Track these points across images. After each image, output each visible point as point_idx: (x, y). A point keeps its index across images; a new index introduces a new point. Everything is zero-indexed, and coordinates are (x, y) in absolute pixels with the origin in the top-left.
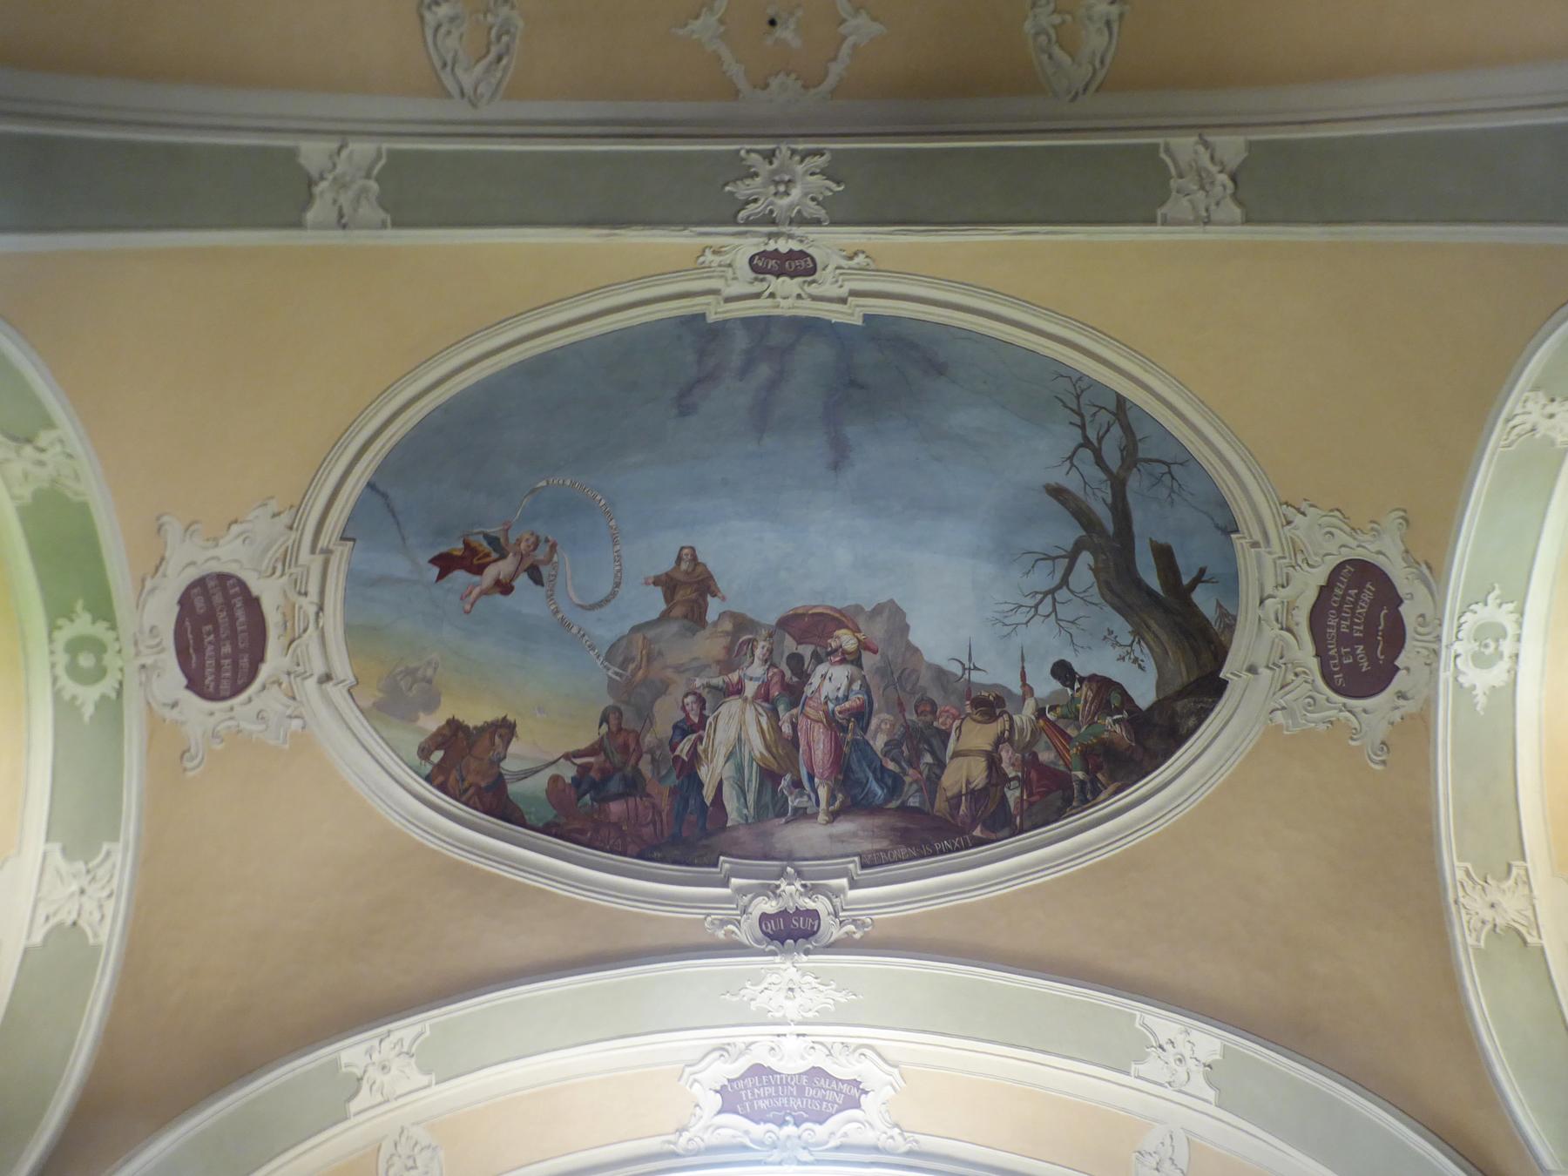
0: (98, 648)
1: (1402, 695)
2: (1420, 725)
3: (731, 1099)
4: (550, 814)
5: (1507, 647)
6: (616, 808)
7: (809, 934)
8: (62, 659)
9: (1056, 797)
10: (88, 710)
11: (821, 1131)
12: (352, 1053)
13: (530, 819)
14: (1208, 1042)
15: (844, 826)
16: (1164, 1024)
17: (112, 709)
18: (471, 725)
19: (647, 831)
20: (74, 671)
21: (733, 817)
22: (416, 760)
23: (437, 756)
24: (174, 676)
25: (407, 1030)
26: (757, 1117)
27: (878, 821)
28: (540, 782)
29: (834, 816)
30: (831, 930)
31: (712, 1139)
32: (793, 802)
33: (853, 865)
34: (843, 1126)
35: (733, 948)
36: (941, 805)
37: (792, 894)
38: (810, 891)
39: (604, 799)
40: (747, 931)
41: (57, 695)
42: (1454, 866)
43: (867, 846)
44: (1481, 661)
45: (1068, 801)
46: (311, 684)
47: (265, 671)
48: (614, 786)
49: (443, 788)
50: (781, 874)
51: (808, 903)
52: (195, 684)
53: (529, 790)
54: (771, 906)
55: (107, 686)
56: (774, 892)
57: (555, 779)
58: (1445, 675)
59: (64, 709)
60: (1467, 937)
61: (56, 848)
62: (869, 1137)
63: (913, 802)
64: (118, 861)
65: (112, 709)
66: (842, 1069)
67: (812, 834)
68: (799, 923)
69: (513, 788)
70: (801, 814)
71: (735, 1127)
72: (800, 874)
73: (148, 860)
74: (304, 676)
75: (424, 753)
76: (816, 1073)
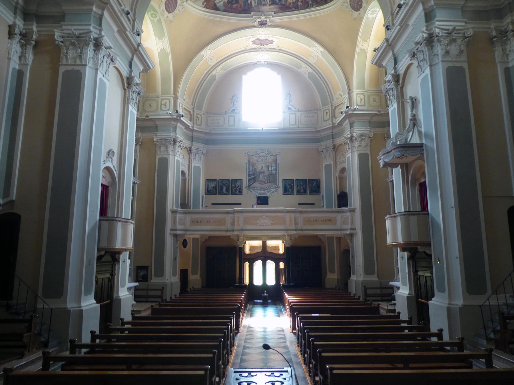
0: (156, 15)
1: (359, 14)
2: (361, 19)
3: (254, 43)
4: (224, 8)
5: (376, 13)
6: (234, 6)
7: (265, 24)
8: (150, 16)
9: (306, 5)
10: (156, 21)
11: (267, 46)
12: (202, 53)
13: (221, 9)
14: (322, 49)
15: (272, 7)
16: (316, 45)
17: (159, 21)
18: (243, 120)
19: (240, 9)
20: (152, 17)
21: (253, 6)
22: (202, 5)
23: (205, 4)
24: (166, 13)
25: (208, 47)
26: (258, 45)
27: (277, 6)
28: (222, 3)
29: (270, 5)
30: (269, 23)
31: (251, 48)
32: (263, 3)
33: (273, 13)
34: (270, 46)
35: (254, 27)
36: (287, 4)
37: (263, 18)
38: (266, 18)
39: (232, 5)
40: (256, 24)
41: (150, 20)
42: (359, 40)
43: (275, 10)
44: (372, 14)
45: (308, 6)
46: (185, 3)
47: (178, 5)
48: (234, 2)
49: (207, 8)
50: (261, 15)
51: (265, 20)
52: (169, 12)
53: (220, 5)
54: (260, 20)
55: (158, 18)
56: (260, 18)
57: (224, 2)
58: (365, 16)
59: (152, 21)
60: (357, 50)
61: (157, 38)
62: (274, 47)
63: (283, 3)
64: (166, 39)
65: (159, 21)
66: (270, 39)
67: (266, 8)
68: (264, 22)
69: (218, 5)
70: (265, 5)
71: (255, 46)
72: (264, 15)
73: (170, 38)
74: (183, 2)
75: (203, 4)
76: (266, 39)
